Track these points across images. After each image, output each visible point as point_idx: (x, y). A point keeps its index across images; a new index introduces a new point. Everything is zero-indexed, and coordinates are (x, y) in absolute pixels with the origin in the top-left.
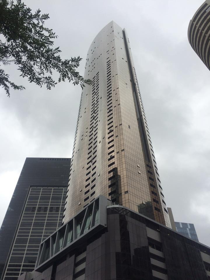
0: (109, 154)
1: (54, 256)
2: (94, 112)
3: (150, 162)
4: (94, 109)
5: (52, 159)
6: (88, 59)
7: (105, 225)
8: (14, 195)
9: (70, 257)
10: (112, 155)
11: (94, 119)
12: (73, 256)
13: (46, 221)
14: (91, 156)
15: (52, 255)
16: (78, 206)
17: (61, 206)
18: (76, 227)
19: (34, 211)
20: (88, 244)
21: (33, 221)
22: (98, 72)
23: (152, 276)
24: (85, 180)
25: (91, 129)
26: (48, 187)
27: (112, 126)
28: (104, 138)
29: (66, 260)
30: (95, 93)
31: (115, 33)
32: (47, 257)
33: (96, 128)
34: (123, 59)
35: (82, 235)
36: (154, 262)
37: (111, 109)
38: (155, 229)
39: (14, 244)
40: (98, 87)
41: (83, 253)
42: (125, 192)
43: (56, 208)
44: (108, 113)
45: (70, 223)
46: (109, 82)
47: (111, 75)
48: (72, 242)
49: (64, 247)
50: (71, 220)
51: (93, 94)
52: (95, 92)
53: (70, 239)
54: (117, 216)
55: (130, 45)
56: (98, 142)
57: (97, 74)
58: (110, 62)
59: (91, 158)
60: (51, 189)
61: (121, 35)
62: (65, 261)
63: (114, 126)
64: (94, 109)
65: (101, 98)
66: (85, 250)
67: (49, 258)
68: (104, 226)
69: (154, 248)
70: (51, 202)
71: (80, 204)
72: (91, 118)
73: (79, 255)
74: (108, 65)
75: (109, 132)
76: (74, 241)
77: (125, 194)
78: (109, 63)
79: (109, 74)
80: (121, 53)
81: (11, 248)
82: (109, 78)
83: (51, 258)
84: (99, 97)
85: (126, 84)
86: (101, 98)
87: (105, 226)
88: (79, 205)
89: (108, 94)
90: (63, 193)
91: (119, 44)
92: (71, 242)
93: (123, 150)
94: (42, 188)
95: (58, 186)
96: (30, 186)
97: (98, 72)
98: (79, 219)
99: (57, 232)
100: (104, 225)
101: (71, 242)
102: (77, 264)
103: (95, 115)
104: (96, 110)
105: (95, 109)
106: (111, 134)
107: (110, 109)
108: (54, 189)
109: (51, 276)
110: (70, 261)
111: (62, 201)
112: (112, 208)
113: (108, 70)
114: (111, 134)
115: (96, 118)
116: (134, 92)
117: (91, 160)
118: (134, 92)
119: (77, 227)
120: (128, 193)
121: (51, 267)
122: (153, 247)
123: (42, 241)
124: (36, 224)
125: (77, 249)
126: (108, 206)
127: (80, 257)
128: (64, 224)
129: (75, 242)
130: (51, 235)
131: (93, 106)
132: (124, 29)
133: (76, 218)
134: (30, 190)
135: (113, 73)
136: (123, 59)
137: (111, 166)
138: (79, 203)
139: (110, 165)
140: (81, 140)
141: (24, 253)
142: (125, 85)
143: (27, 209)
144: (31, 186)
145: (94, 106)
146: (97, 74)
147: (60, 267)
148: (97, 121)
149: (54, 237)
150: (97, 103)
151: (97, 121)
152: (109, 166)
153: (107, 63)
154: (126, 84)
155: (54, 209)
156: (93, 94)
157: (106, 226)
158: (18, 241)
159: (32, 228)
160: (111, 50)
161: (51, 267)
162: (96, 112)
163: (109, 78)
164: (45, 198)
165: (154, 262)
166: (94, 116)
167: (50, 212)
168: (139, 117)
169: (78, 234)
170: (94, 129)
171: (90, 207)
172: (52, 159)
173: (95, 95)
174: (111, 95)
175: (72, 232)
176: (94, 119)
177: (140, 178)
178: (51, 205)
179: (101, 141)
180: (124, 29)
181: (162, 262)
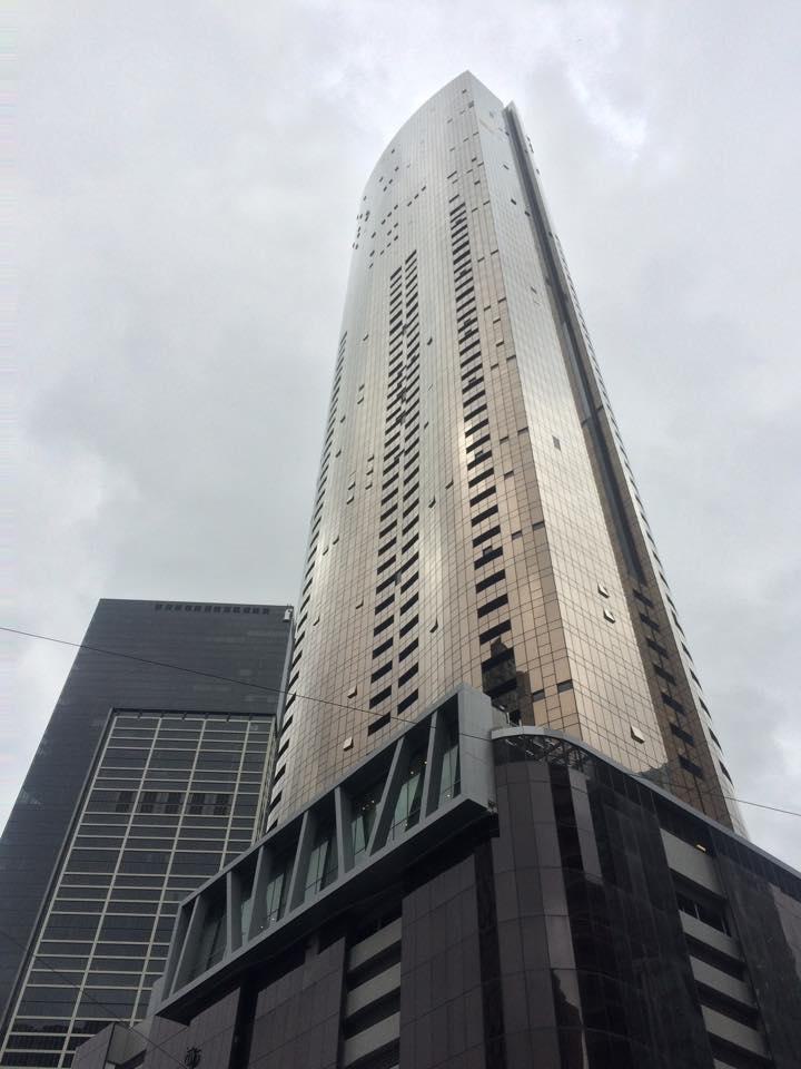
0: (477, 542)
1: (247, 946)
2: (399, 397)
3: (645, 583)
4: (400, 386)
5: (203, 609)
6: (368, 213)
7: (491, 805)
8: (48, 745)
9: (320, 951)
10: (491, 547)
11: (399, 421)
12: (339, 945)
13: (174, 850)
14: (393, 559)
15: (350, 865)
16: (340, 752)
17: (236, 793)
18: (443, 754)
19: (127, 808)
20: (409, 890)
21: (122, 849)
22: (415, 252)
23: (704, 1029)
24: (371, 650)
25: (391, 460)
26: (185, 717)
27: (487, 438)
28: (452, 483)
29: (302, 962)
30: (400, 329)
31: (481, 112)
32: (210, 959)
33: (412, 454)
34: (515, 203)
35: (381, 850)
36: (704, 972)
37: (494, 542)
38: (692, 841)
39: (40, 940)
40: (417, 305)
41: (383, 926)
42: (558, 685)
43: (215, 797)
44: (464, 391)
45: (321, 812)
46: (464, 279)
47: (473, 257)
48: (326, 889)
49: (375, 849)
50: (294, 818)
51: (392, 332)
52: (404, 323)
53: (320, 876)
54: (539, 772)
55: (537, 160)
56: (425, 500)
57: (410, 258)
58: (462, 209)
59: (393, 565)
60: (199, 725)
61: (501, 123)
62: (302, 967)
63: (495, 438)
64: (400, 386)
65: (429, 344)
66: (396, 913)
67: (335, 878)
68: (485, 809)
69: (696, 917)
70: (197, 775)
71: (351, 746)
72: (388, 419)
73: (359, 941)
74: (454, 223)
75: (473, 459)
76: (425, 822)
77: (559, 691)
78: (458, 213)
79: (461, 252)
80: (505, 183)
81: (30, 954)
82: (461, 267)
83: (230, 956)
84: (423, 340)
85: (532, 289)
86: (429, 344)
87: (490, 810)
88: (346, 749)
89: (461, 324)
90: (246, 742)
91: (497, 150)
92: (322, 888)
93: (538, 524)
94: (205, 721)
95: (181, 712)
96: (111, 710)
97: (415, 252)
98: (363, 787)
99: (195, 898)
100: (484, 804)
101: (322, 888)
102: (353, 979)
103: (405, 407)
104: (407, 390)
105: (406, 384)
106: (480, 469)
107: (471, 377)
108: (209, 725)
109: (232, 1031)
110: (322, 965)
111: (240, 771)
112: (510, 738)
113: (455, 239)
114: (480, 469)
115: (408, 418)
116: (562, 323)
117: (392, 574)
118: (565, 324)
119: (353, 825)
120: (572, 687)
121: (234, 998)
122: (692, 913)
123: (225, 865)
124: (131, 861)
125: (348, 916)
126: (494, 729)
127: (368, 949)
128: (279, 823)
129: (425, 826)
130: (197, 891)
131: (396, 375)
132: (512, 104)
133: (346, 786)
134: (113, 727)
135: (477, 249)
136: (515, 203)
137: (492, 577)
138: (347, 743)
139: (376, 673)
140: (345, 505)
141: (13, 1030)
142: (530, 295)
143: (99, 800)
144: (114, 710)
145: (400, 375)
146: (410, 258)
147: (268, 999)
148: (418, 427)
149: (244, 872)
150: (414, 360)
151: (418, 427)
152: (481, 587)
153: (451, 214)
154: (532, 289)
155: (158, 799)
156: (392, 332)
157: (495, 810)
158: (59, 927)
159: (115, 874)
160: (470, 168)
161: (234, 998)
162: (408, 395)
163: (461, 267)
164: (173, 759)
165: (704, 972)
166: (399, 409)
167: (191, 812)
168: (589, 415)
169: (357, 854)
170: (404, 460)
171: (416, 737)
172: (203, 609)
173: (402, 333)
174: (473, 327)
175: (414, 783)
176: (399, 421)
177: (613, 639)
178: (194, 786)
179: (321, 620)
180: (512, 104)
181: (734, 976)
